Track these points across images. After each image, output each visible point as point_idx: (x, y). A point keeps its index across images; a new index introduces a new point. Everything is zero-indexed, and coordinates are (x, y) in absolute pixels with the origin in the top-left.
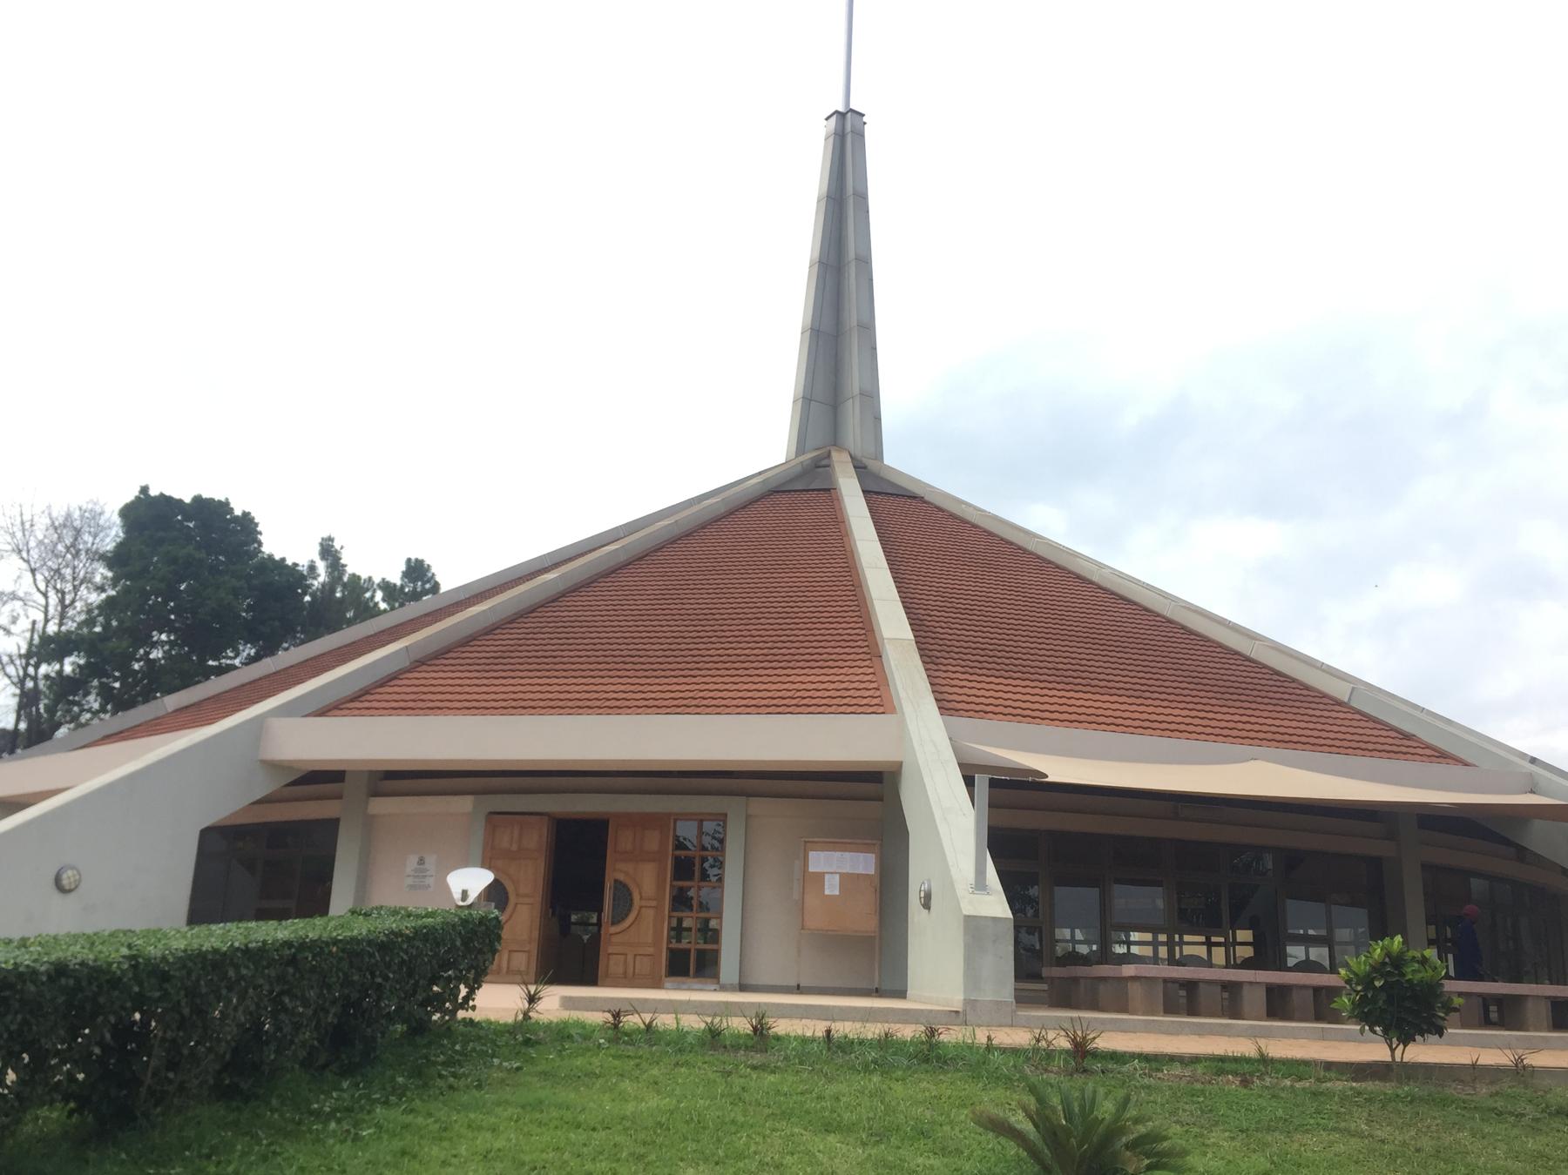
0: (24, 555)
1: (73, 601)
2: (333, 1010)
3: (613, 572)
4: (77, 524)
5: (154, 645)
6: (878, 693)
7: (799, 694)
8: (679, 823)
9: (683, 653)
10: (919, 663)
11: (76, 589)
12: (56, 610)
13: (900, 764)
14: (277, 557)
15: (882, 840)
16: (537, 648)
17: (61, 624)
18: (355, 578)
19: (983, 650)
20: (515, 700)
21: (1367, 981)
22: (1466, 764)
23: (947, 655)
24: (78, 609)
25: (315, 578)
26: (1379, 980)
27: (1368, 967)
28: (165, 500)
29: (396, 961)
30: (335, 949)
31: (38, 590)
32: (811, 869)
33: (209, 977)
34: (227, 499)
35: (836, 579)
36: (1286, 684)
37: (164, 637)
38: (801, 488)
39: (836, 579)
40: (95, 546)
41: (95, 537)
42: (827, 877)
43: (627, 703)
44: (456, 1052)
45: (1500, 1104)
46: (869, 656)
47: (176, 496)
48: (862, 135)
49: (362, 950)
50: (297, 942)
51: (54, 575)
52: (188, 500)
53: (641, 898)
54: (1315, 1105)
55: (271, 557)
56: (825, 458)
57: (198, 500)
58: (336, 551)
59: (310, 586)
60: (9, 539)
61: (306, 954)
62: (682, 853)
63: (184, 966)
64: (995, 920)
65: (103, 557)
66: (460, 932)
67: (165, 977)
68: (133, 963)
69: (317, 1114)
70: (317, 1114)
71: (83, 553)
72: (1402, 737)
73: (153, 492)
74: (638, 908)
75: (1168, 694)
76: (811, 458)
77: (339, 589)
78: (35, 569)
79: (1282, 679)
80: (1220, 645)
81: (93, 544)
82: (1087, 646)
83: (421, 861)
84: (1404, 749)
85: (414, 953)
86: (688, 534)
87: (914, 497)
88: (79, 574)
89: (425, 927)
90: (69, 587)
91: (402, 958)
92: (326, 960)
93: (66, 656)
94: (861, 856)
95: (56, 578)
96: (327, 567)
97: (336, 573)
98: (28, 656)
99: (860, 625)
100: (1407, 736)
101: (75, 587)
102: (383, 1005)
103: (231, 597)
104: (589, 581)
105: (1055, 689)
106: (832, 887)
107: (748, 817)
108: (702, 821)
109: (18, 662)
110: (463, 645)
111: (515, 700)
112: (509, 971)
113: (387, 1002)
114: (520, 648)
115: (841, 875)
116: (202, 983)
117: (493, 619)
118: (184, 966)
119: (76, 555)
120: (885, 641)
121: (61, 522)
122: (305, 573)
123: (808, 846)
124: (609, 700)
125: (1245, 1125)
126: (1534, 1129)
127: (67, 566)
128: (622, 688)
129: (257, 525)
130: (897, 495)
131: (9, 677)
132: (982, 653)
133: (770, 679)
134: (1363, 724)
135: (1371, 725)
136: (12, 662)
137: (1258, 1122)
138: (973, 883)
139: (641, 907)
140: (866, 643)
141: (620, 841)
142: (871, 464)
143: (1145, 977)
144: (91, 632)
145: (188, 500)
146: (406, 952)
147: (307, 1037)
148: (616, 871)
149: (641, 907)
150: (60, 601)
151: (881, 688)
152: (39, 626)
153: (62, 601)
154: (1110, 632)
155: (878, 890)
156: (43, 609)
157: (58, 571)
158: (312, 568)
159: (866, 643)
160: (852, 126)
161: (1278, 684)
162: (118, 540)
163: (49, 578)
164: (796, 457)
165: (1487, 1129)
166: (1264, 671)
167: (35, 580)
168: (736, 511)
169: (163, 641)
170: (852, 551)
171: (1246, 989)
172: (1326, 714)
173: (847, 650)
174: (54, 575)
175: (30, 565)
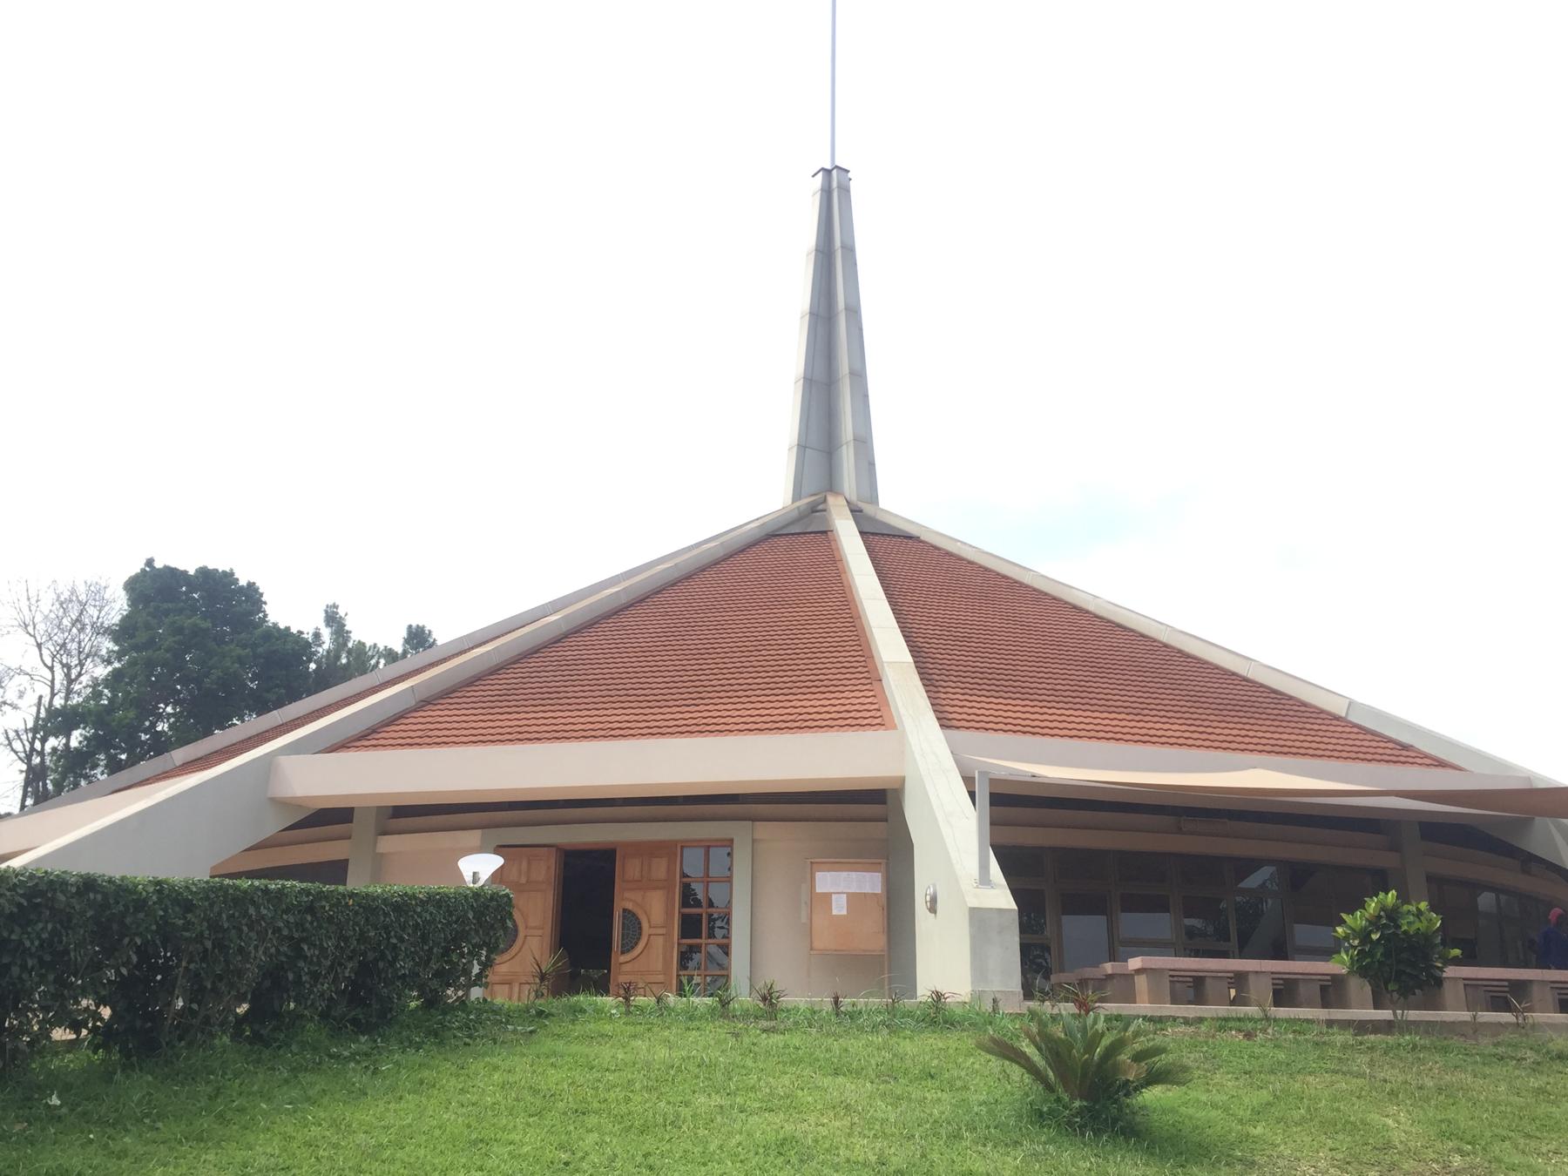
0: (30, 629)
1: (80, 675)
2: (350, 965)
3: (615, 613)
4: (83, 598)
5: (160, 717)
6: (879, 714)
7: (801, 717)
8: (685, 850)
9: (683, 696)
10: (919, 683)
11: (81, 664)
12: (62, 684)
13: (903, 780)
14: (282, 626)
15: (888, 859)
16: (540, 685)
17: (67, 698)
18: (361, 644)
19: (982, 673)
20: (520, 733)
21: (1364, 935)
23: (946, 679)
24: (84, 684)
25: (320, 645)
26: (1376, 933)
27: (1364, 922)
28: (171, 572)
29: (411, 924)
30: (351, 902)
31: (45, 665)
32: (818, 890)
33: (231, 912)
34: (232, 570)
35: (837, 644)
36: (1283, 701)
37: (169, 709)
38: (797, 531)
39: (837, 644)
40: (100, 620)
41: (100, 611)
42: (834, 896)
43: (632, 732)
44: (471, 1020)
45: (1501, 1050)
46: (869, 681)
47: (181, 568)
48: (848, 191)
49: (377, 907)
50: (315, 890)
51: (60, 650)
52: (192, 572)
53: (650, 927)
54: (1317, 1053)
55: (275, 625)
56: (822, 503)
57: (204, 572)
58: (341, 617)
59: (314, 653)
60: (16, 616)
61: (324, 903)
62: (685, 880)
63: (207, 898)
64: (1000, 911)
65: (108, 631)
66: (472, 905)
67: (188, 906)
68: (158, 888)
69: (336, 1057)
70: (336, 1057)
71: (89, 627)
72: (1400, 748)
73: (158, 564)
74: (652, 929)
75: (1167, 711)
76: (807, 503)
77: (344, 655)
78: (41, 644)
79: (1279, 697)
80: (1217, 667)
81: (98, 618)
82: (1085, 669)
84: (1402, 759)
85: (428, 918)
86: (689, 577)
87: (910, 537)
88: (84, 649)
89: (438, 894)
90: (75, 661)
91: (416, 920)
92: (342, 912)
93: (73, 730)
94: (867, 875)
95: (62, 652)
96: (332, 634)
97: (341, 639)
98: (35, 730)
99: (860, 653)
100: (1405, 747)
101: (80, 661)
102: (399, 966)
103: (237, 665)
104: (592, 622)
105: (1054, 708)
106: (839, 907)
107: (754, 841)
108: (709, 847)
109: (24, 737)
110: (469, 685)
111: (520, 733)
113: (402, 963)
114: (525, 686)
115: (849, 895)
116: (224, 916)
117: (495, 661)
118: (207, 898)
119: (82, 630)
120: (885, 665)
121: (67, 597)
122: (310, 640)
123: (814, 867)
124: (614, 729)
125: (1248, 1068)
126: (1536, 1068)
127: (73, 640)
128: (627, 718)
129: (261, 595)
130: (889, 535)
131: (16, 753)
132: (981, 676)
133: (772, 705)
134: (1361, 737)
135: (1369, 737)
136: (18, 735)
137: (1262, 1066)
138: (977, 878)
139: (650, 935)
140: (866, 669)
141: (628, 870)
142: (868, 509)
143: (1151, 969)
144: (97, 704)
145: (192, 572)
146: (420, 916)
147: (325, 988)
148: (624, 900)
149: (650, 935)
150: (66, 675)
151: (882, 709)
152: (46, 701)
153: (68, 675)
154: (1108, 656)
155: (885, 909)
156: (50, 684)
157: (64, 645)
158: (317, 635)
159: (866, 669)
160: (839, 182)
161: (1276, 701)
162: (125, 613)
163: (55, 653)
164: (793, 503)
165: (1487, 1070)
166: (1261, 689)
167: (41, 655)
168: (736, 554)
169: (169, 714)
170: (850, 586)
171: (1251, 978)
172: (1324, 728)
173: (847, 676)
174: (60, 650)
175: (36, 640)
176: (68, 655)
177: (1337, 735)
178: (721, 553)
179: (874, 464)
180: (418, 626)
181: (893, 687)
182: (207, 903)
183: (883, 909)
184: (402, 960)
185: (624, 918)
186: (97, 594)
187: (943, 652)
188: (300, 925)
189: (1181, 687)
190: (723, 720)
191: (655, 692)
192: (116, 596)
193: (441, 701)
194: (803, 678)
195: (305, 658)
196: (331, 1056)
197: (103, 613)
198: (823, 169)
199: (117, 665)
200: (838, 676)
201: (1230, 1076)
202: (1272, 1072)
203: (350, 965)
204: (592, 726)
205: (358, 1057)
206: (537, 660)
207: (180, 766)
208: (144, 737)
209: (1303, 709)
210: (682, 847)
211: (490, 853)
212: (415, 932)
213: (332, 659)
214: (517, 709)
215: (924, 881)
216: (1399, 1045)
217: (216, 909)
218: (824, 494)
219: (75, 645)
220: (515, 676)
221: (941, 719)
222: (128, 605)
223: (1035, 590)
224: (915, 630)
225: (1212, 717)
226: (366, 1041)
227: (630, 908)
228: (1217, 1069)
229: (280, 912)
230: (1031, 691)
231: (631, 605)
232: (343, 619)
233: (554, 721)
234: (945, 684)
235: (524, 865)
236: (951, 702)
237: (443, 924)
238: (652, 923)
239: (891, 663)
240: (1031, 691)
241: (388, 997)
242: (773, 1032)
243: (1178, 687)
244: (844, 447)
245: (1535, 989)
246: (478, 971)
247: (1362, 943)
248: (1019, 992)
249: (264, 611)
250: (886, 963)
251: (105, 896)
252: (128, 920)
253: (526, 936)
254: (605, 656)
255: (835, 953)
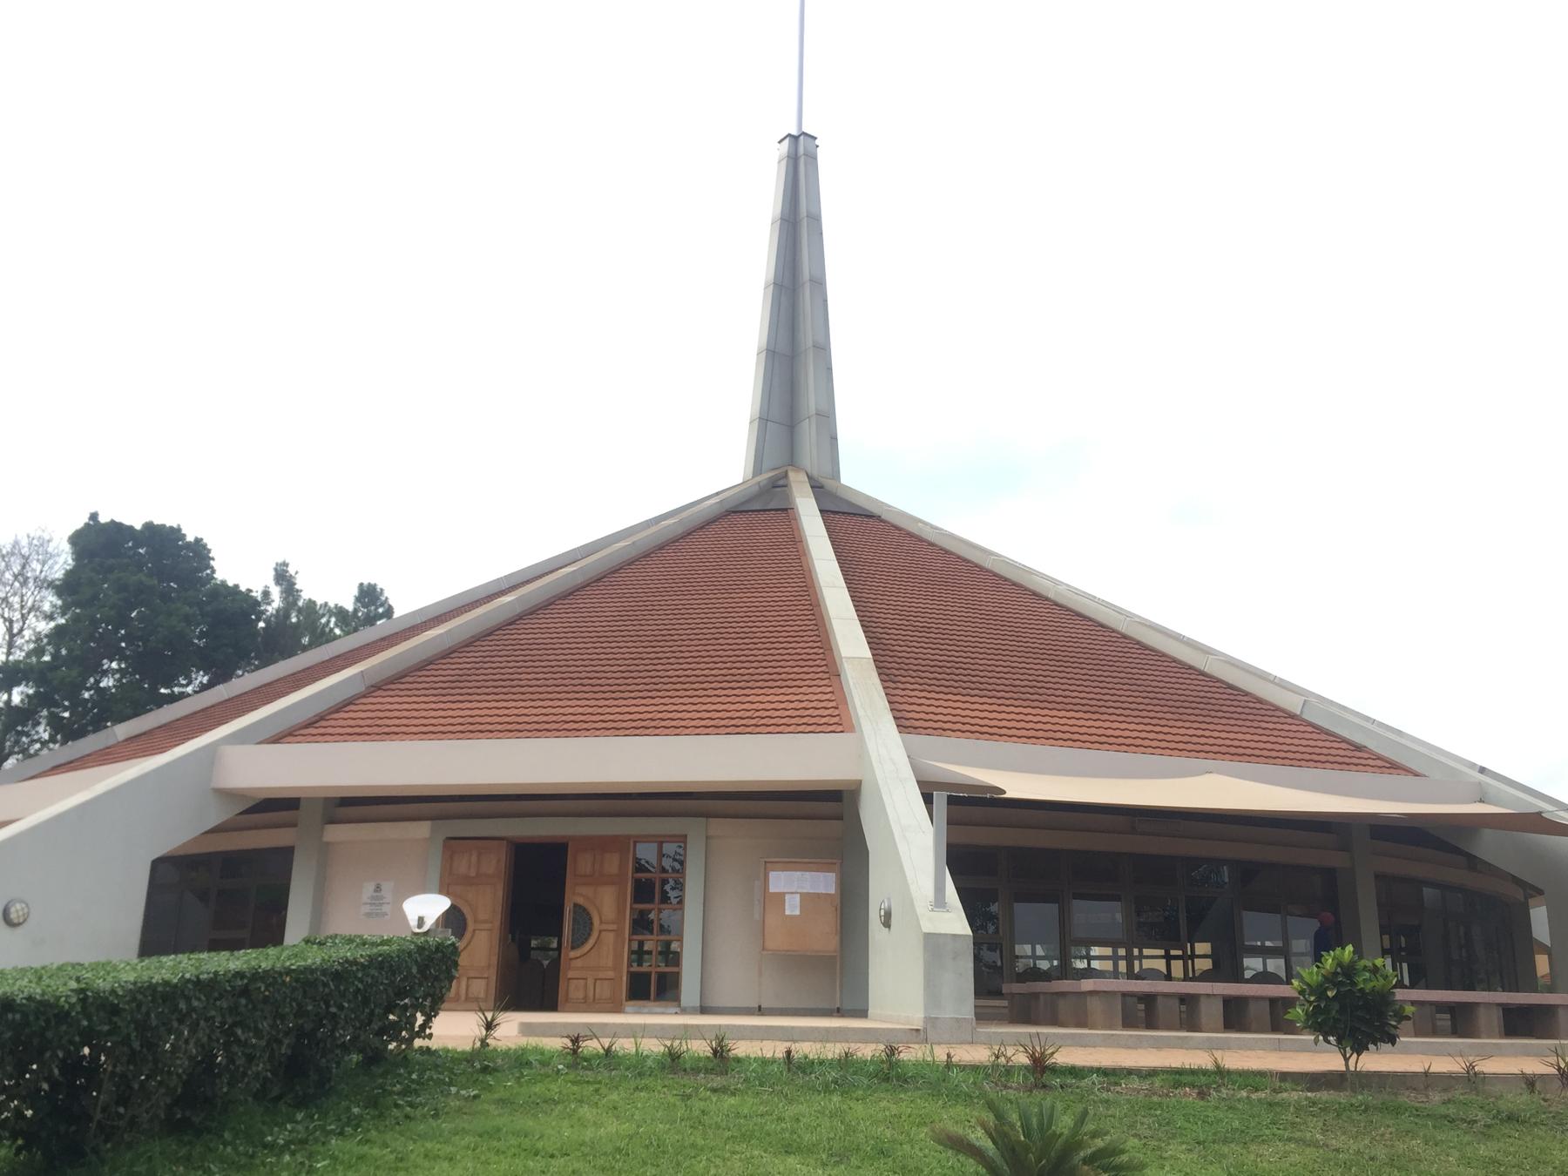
1: (21, 630)
4: (25, 551)
5: (105, 673)
6: (837, 712)
7: (757, 714)
10: (877, 681)
11: (24, 618)
13: (859, 783)
14: (230, 584)
18: (311, 603)
22: (1417, 775)
24: (27, 638)
25: (269, 604)
26: (1332, 990)
28: (116, 528)
30: (288, 979)
34: (179, 525)
37: (114, 665)
38: (758, 508)
40: (43, 574)
42: (787, 897)
43: (585, 726)
47: (127, 522)
52: (138, 527)
53: (601, 922)
55: (224, 584)
57: (149, 527)
63: (134, 999)
64: (955, 936)
65: (51, 585)
66: (417, 960)
67: (115, 1010)
68: (81, 996)
69: (270, 1147)
72: (1353, 748)
73: (103, 519)
76: (770, 478)
77: (293, 615)
79: (1236, 693)
80: (1175, 660)
81: (41, 572)
83: (378, 888)
86: (646, 555)
87: (871, 516)
89: (380, 955)
90: (17, 616)
91: (357, 986)
94: (821, 875)
96: (282, 592)
99: (819, 644)
100: (1359, 748)
101: (23, 615)
102: (338, 1035)
106: (792, 907)
107: (707, 837)
112: (467, 999)
117: (449, 643)
118: (134, 999)
119: (24, 583)
120: (844, 660)
121: (9, 550)
122: (259, 599)
123: (768, 866)
126: (1486, 1134)
134: (1314, 736)
135: (1323, 737)
141: (580, 864)
142: (829, 484)
143: (1105, 992)
144: (39, 662)
145: (138, 527)
146: (361, 981)
147: (260, 1069)
148: (576, 895)
151: (840, 707)
158: (266, 594)
159: (824, 663)
162: (68, 568)
164: (753, 477)
166: (1218, 684)
176: (9, 609)
177: (1292, 734)
178: (680, 530)
179: (836, 439)
180: (369, 584)
181: (851, 684)
182: (134, 1004)
183: (836, 910)
184: (342, 1028)
185: (575, 913)
186: (41, 547)
187: (902, 643)
188: (233, 1010)
189: (1138, 682)
190: (679, 715)
191: (610, 682)
192: (61, 548)
193: (393, 686)
194: (760, 671)
195: (253, 617)
196: (265, 1146)
197: (46, 567)
198: (789, 135)
199: (62, 621)
200: (795, 670)
201: (1184, 1147)
202: (1225, 1141)
203: (286, 1041)
204: (545, 718)
205: (293, 1147)
206: (491, 643)
207: (124, 741)
208: (86, 695)
209: (1258, 706)
210: (635, 843)
211: (435, 893)
212: (355, 997)
213: (282, 618)
214: (470, 698)
215: (879, 892)
216: (1352, 1105)
217: (144, 1009)
218: (784, 469)
219: (17, 599)
220: (468, 660)
221: (898, 718)
222: (73, 559)
223: (995, 575)
224: (874, 619)
225: (1169, 716)
226: (303, 1118)
227: (581, 903)
228: (1171, 1138)
229: (212, 1001)
230: (990, 687)
231: (588, 585)
232: (294, 577)
233: (506, 712)
234: (903, 680)
235: (474, 858)
236: (909, 699)
237: (386, 984)
238: (603, 918)
239: (849, 658)
240: (990, 687)
241: (327, 1067)
242: (723, 1092)
243: (1136, 666)
244: (805, 424)
245: (1482, 1011)
246: (422, 1022)
247: (1319, 999)
248: (972, 1019)
249: (212, 567)
250: (838, 963)
251: (25, 1015)
252: (49, 1035)
253: (474, 930)
254: (564, 625)
255: (789, 953)
